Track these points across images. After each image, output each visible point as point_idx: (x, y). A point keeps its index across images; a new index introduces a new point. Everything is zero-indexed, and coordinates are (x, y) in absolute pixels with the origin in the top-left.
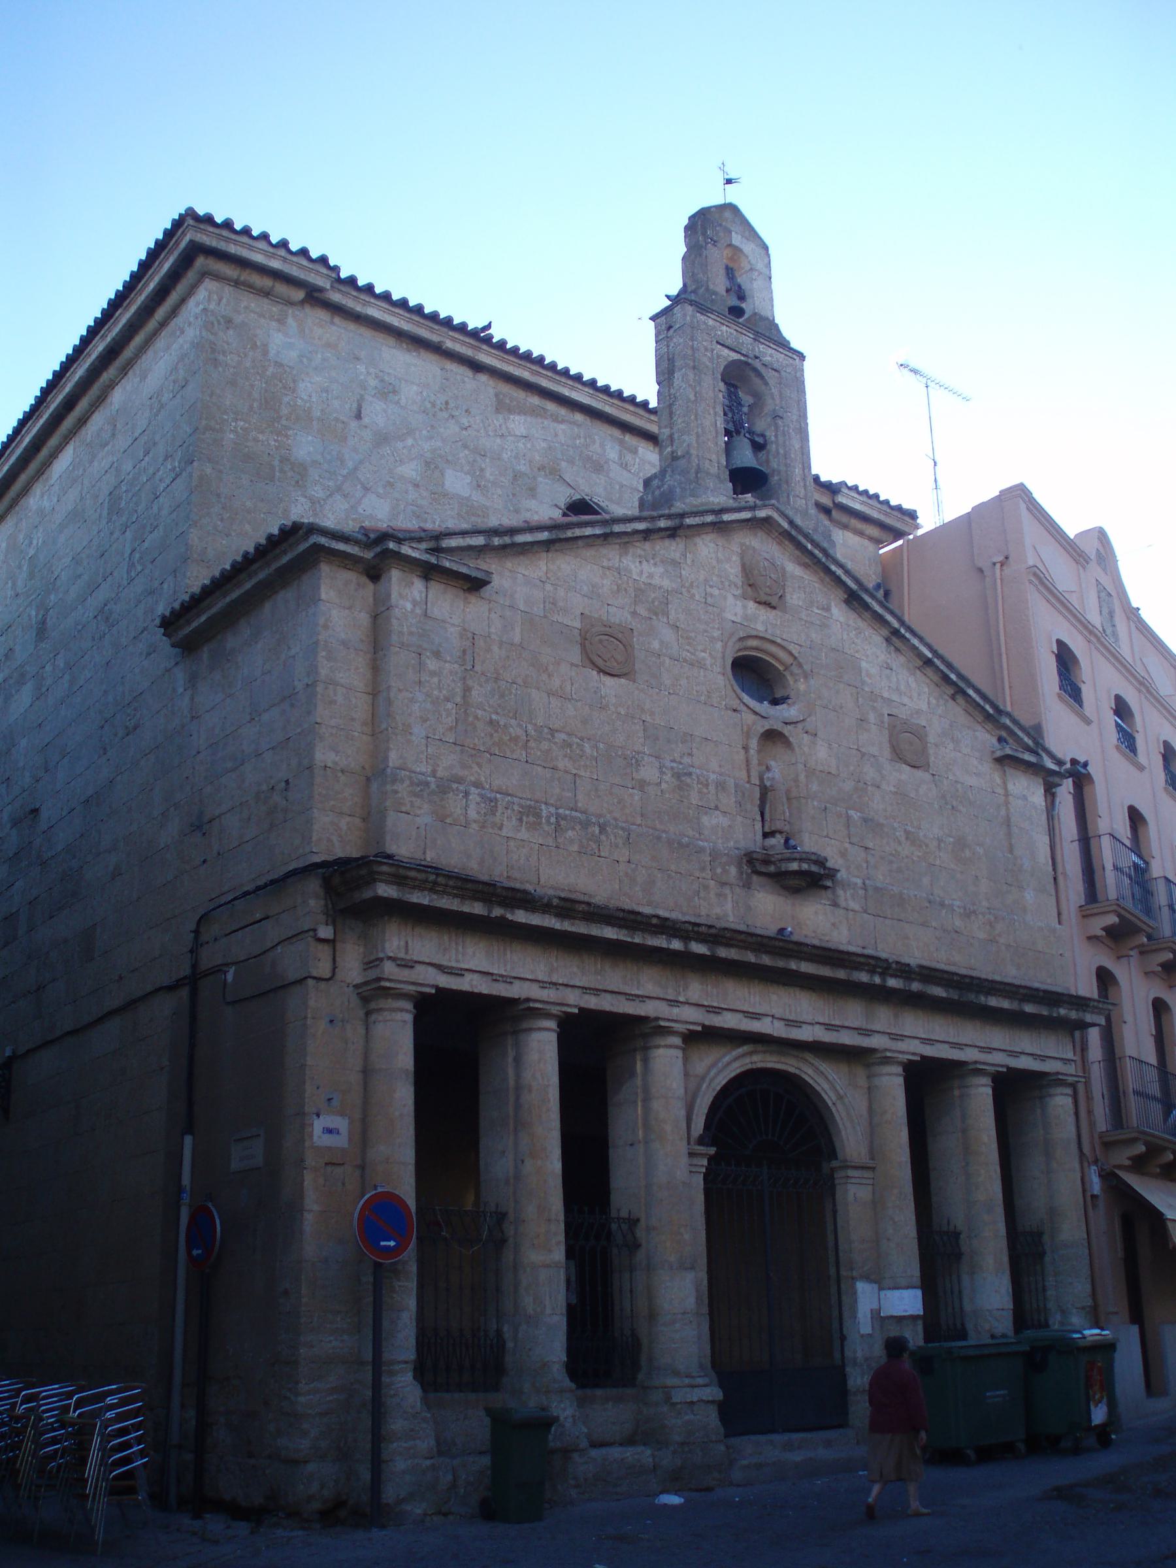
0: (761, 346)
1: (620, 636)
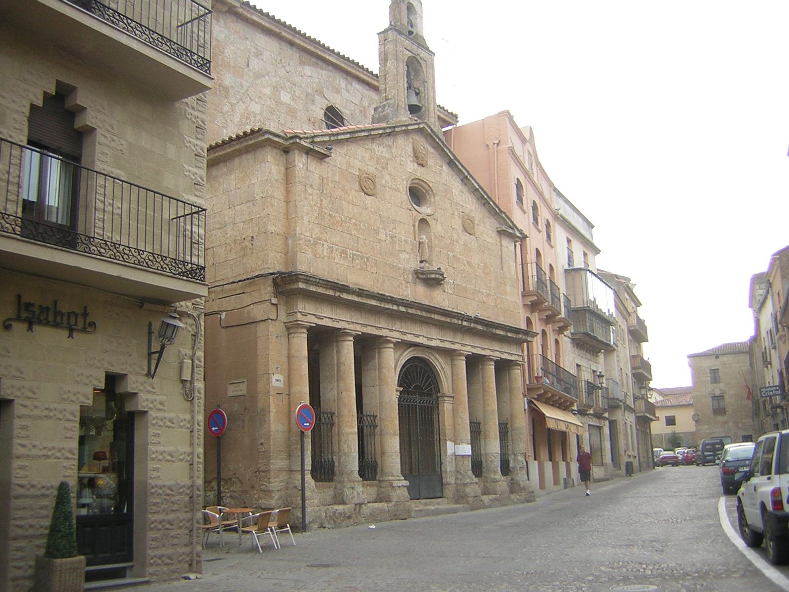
1: (372, 178)
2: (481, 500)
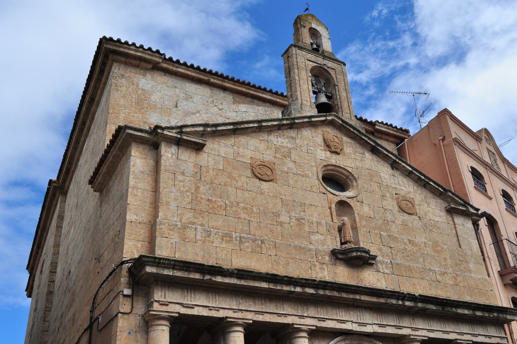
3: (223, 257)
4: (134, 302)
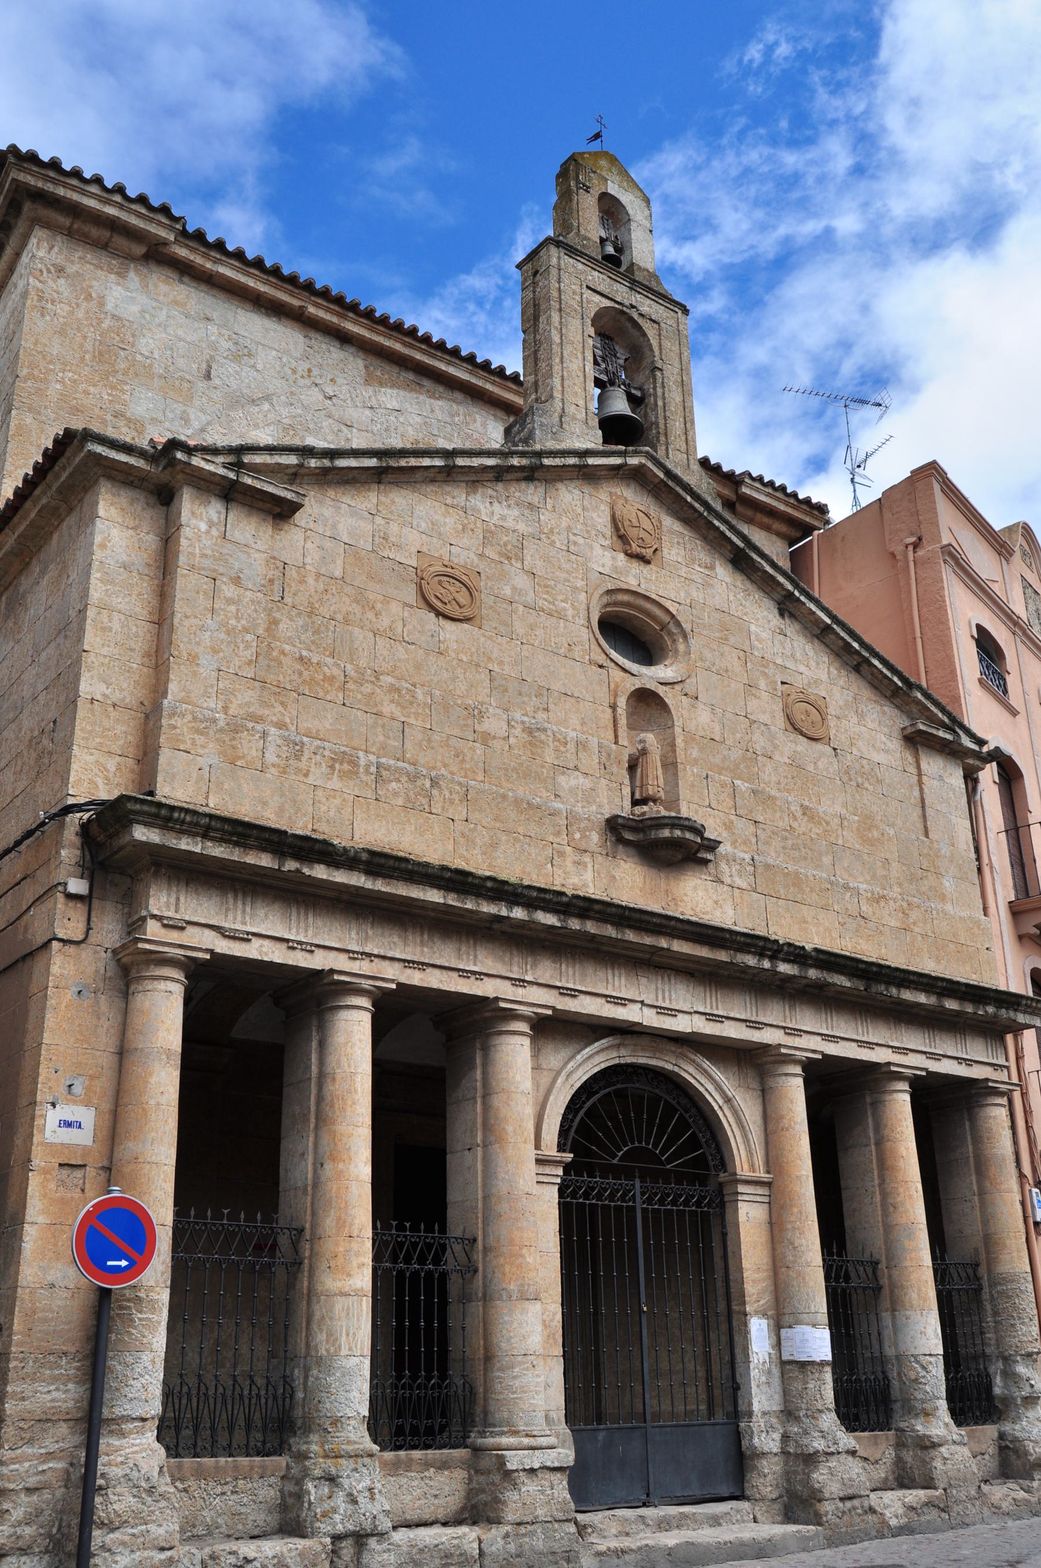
0: (638, 296)
2: (872, 1510)
3: (331, 814)
4: (93, 914)
